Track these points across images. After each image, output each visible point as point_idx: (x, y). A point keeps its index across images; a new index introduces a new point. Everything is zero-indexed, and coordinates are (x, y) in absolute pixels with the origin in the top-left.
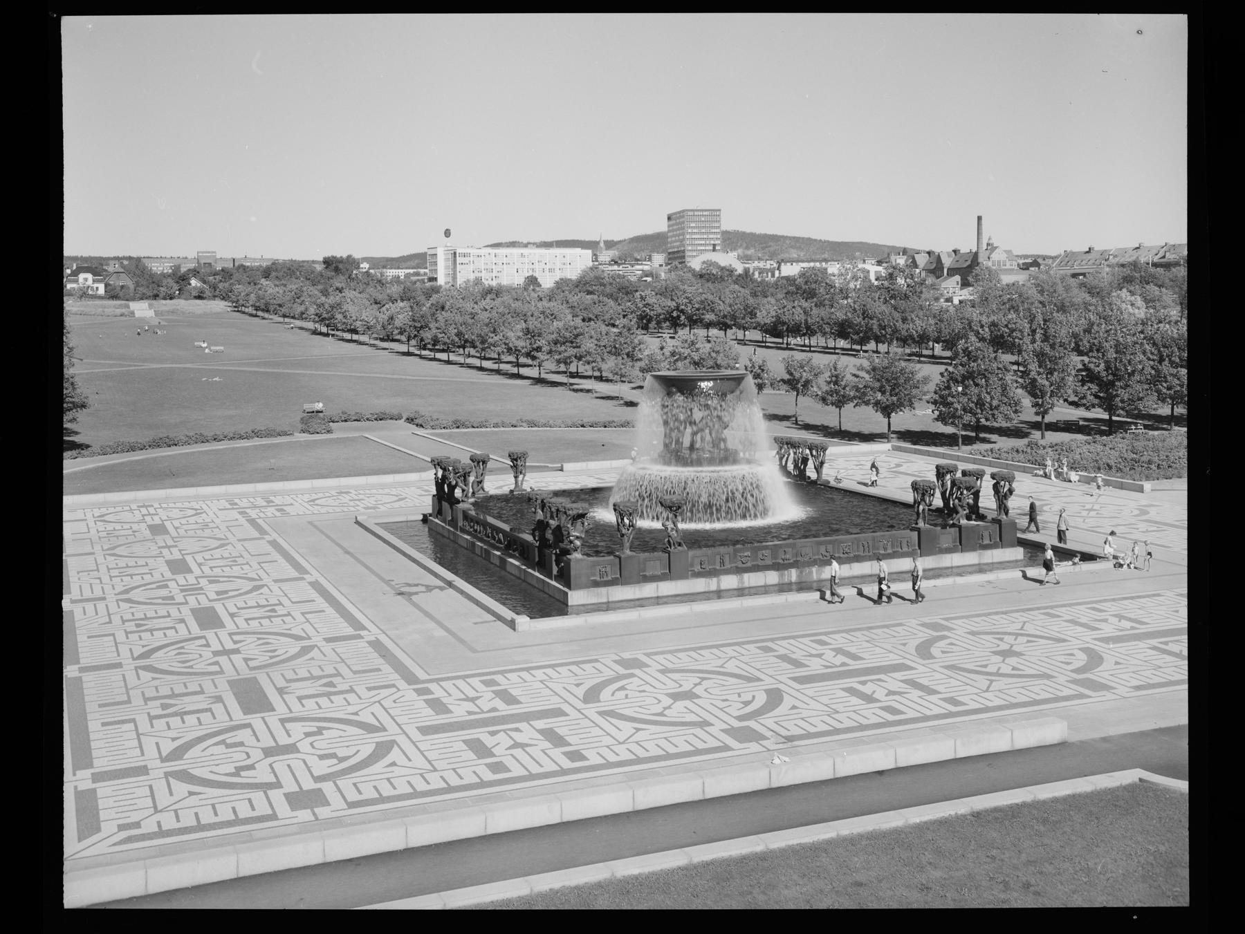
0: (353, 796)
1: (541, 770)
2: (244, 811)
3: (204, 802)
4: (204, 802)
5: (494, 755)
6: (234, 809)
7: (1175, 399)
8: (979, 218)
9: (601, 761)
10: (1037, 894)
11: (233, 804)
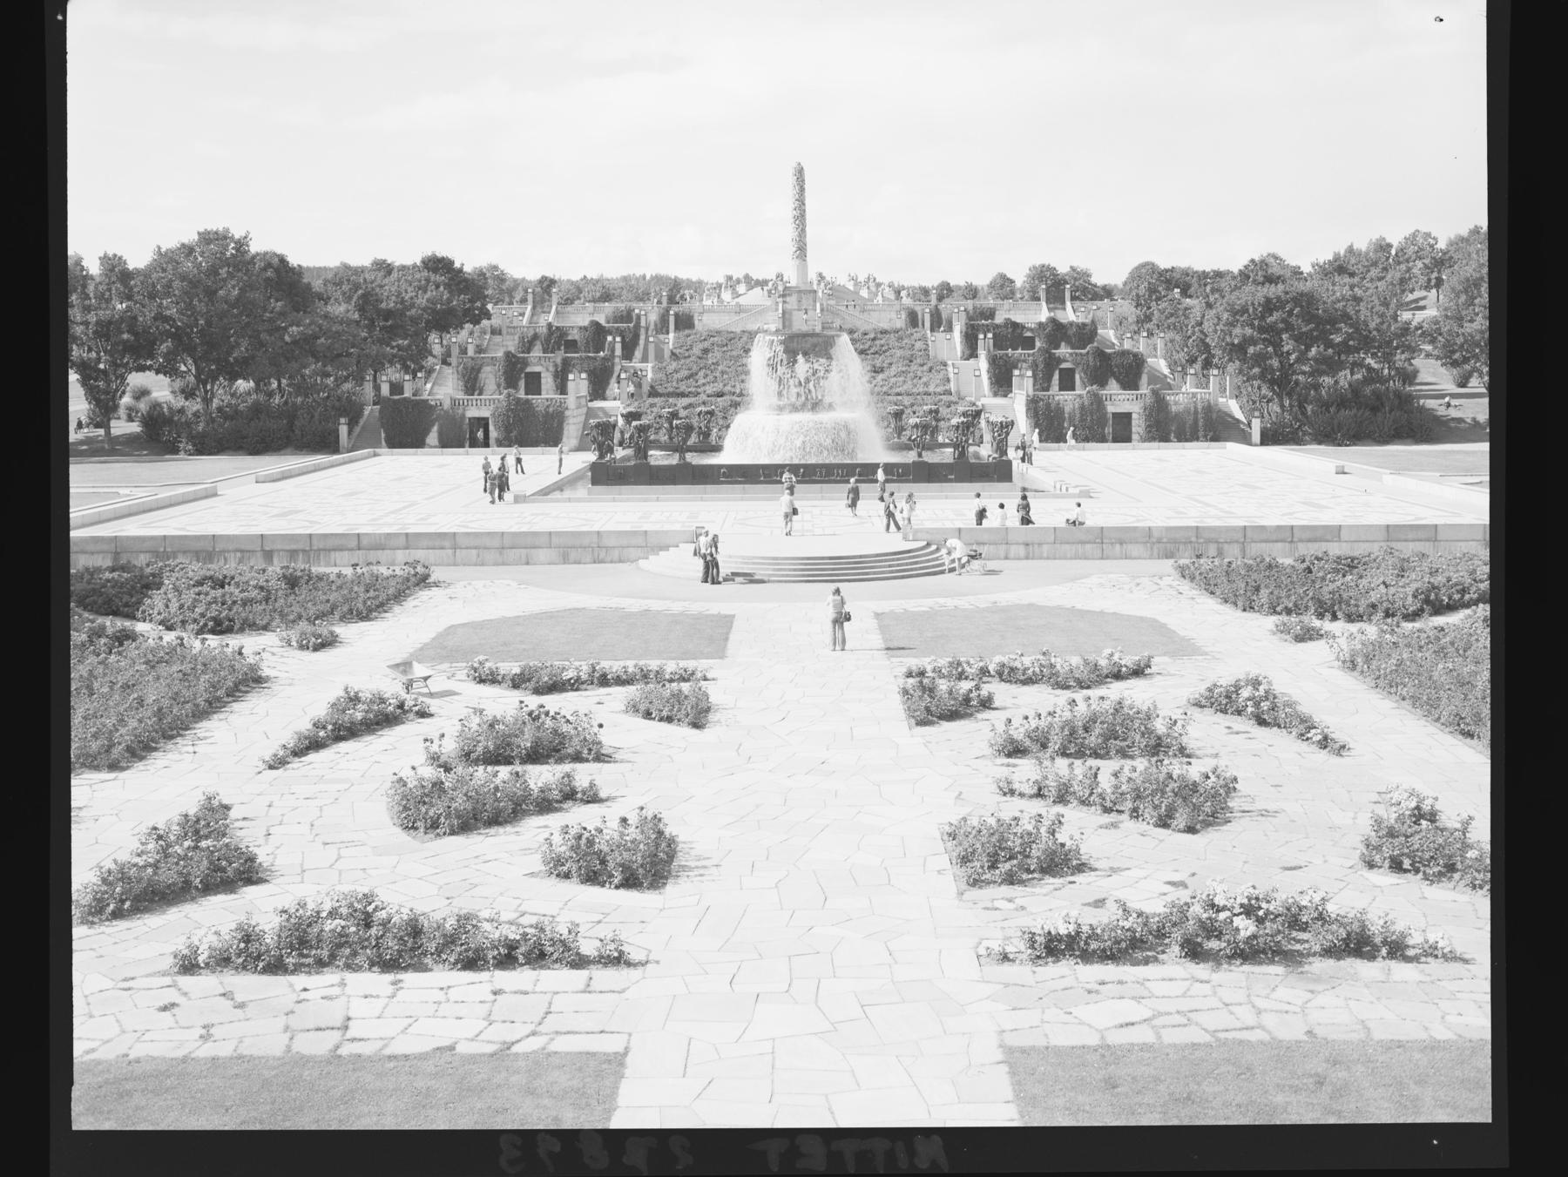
8: (800, 173)
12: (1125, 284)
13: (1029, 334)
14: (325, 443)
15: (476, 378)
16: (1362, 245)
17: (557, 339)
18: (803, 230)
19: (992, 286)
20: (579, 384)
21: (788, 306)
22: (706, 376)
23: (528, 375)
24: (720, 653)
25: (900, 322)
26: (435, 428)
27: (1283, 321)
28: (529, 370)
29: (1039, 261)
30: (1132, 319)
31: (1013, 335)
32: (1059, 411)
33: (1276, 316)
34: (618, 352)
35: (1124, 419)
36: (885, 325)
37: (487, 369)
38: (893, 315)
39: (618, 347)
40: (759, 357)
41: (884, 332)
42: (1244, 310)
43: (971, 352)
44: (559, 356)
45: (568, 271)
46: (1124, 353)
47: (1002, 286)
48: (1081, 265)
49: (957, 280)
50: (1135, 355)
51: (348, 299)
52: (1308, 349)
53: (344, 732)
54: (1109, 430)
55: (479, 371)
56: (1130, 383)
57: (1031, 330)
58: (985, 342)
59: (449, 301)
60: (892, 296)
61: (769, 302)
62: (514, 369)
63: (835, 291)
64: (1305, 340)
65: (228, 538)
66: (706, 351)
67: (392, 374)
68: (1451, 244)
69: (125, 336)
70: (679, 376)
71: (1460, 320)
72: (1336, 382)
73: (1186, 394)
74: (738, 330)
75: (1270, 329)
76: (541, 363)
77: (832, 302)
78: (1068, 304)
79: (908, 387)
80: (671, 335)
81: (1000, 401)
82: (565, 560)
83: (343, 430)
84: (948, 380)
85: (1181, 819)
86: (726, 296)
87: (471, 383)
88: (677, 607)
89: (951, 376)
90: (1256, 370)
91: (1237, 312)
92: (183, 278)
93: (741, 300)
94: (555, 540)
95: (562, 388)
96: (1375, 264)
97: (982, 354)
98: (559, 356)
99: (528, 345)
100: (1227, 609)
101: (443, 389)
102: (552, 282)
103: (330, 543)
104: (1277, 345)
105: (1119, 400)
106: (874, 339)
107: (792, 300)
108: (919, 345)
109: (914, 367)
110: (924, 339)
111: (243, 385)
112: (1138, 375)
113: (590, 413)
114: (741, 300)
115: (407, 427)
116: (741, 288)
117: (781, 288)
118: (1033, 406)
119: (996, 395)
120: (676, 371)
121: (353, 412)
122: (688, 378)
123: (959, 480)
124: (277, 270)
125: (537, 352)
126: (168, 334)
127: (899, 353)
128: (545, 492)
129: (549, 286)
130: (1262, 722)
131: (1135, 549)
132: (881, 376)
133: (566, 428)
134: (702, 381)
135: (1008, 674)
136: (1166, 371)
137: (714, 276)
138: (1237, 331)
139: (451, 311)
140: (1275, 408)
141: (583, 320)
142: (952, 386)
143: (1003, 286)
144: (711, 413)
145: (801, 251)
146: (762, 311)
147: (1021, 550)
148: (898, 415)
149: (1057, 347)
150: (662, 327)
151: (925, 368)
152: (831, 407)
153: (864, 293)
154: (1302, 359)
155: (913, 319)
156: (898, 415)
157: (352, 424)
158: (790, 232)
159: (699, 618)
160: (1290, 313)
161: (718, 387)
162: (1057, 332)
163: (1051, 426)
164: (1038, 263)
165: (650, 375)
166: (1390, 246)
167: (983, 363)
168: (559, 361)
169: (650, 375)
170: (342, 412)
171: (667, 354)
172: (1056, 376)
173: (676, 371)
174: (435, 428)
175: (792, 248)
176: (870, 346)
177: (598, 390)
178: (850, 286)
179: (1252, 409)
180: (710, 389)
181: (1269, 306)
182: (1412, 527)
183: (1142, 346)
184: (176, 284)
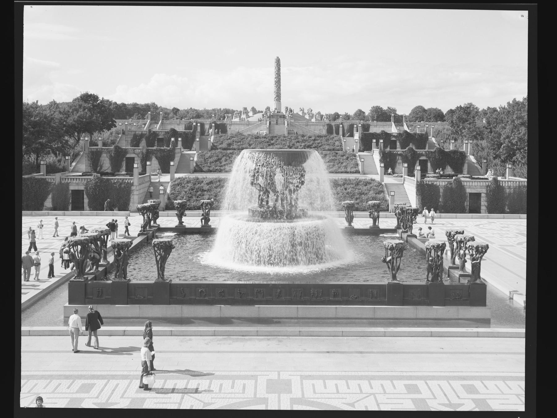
0: (250, 383)
1: (439, 382)
2: (319, 384)
3: (344, 396)
4: (344, 396)
5: (473, 400)
6: (325, 387)
7: (525, 178)
8: (278, 61)
9: (486, 382)
10: (235, 216)
11: (348, 391)
12: (410, 114)
13: (394, 139)
15: (98, 160)
19: (355, 114)
22: (226, 160)
23: (128, 158)
25: (324, 132)
26: (50, 196)
28: (128, 156)
36: (317, 132)
37: (104, 155)
41: (320, 136)
45: (166, 101)
47: (360, 115)
48: (392, 107)
49: (342, 112)
54: (467, 204)
57: (394, 136)
59: (91, 117)
60: (320, 119)
63: (295, 117)
70: (211, 160)
77: (292, 121)
84: (357, 165)
86: (243, 116)
89: (360, 163)
93: (250, 119)
102: (178, 110)
106: (314, 140)
109: (338, 157)
110: (340, 140)
112: (462, 164)
114: (250, 119)
116: (251, 114)
117: (268, 114)
120: (210, 157)
122: (216, 161)
129: (176, 112)
133: (132, 197)
134: (223, 163)
137: (239, 108)
151: (345, 157)
152: (304, 215)
153: (307, 117)
158: (272, 88)
164: (375, 105)
165: (196, 159)
169: (196, 159)
173: (210, 157)
174: (50, 196)
175: (274, 96)
178: (301, 113)
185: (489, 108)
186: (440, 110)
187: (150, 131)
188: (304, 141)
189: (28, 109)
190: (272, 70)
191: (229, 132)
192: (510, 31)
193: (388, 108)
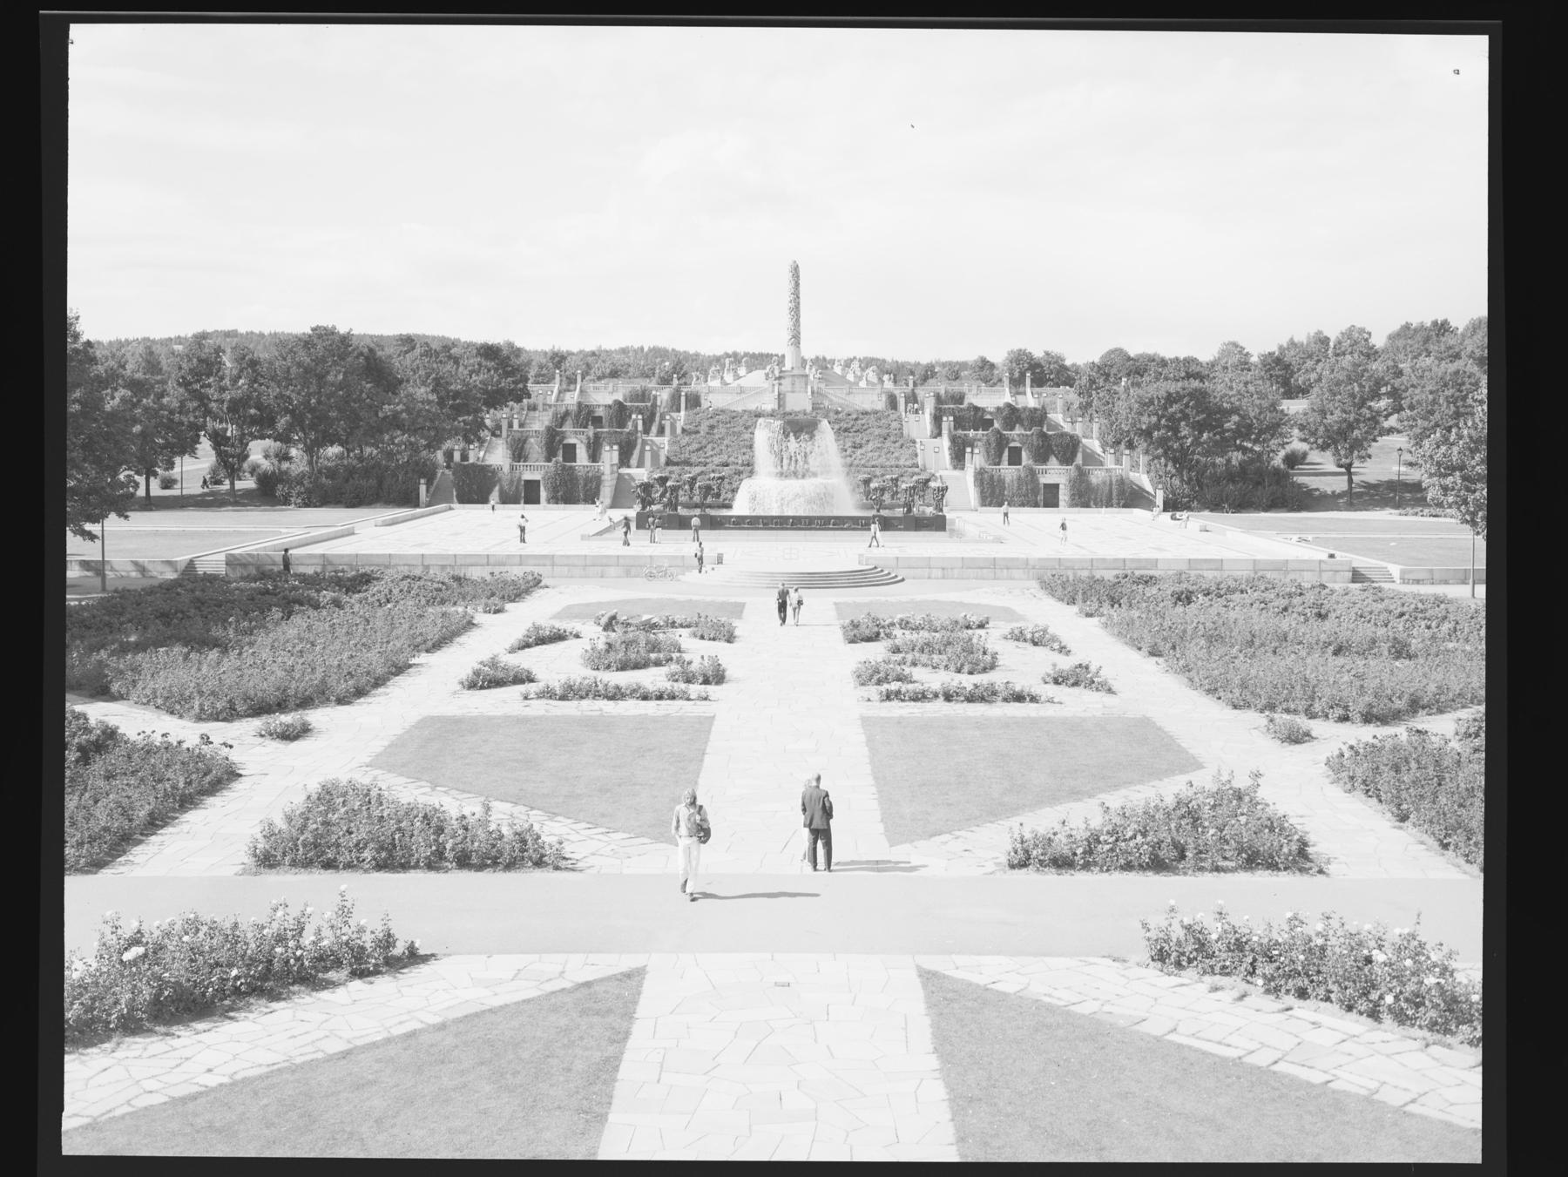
8: (796, 271)
14: (408, 499)
15: (522, 448)
16: (1301, 338)
17: (586, 416)
18: (798, 320)
20: (610, 455)
21: (783, 388)
24: (740, 617)
25: (880, 404)
27: (1181, 411)
29: (1017, 345)
30: (1076, 405)
31: (978, 418)
32: (1001, 481)
33: (1175, 408)
34: (640, 428)
35: (1053, 489)
36: (868, 407)
38: (875, 398)
39: (640, 423)
40: (764, 436)
42: (1151, 402)
43: (938, 434)
44: (590, 431)
46: (1063, 435)
47: (982, 368)
50: (1072, 437)
51: (424, 383)
52: (1201, 433)
53: (541, 641)
54: (1040, 498)
55: (525, 442)
56: (1067, 459)
58: (947, 422)
59: (499, 382)
61: (766, 385)
62: (554, 443)
64: (1200, 427)
65: (400, 556)
66: (712, 427)
67: (455, 445)
68: (1392, 337)
69: (253, 411)
71: (1323, 413)
72: (1229, 461)
73: (1112, 466)
74: (740, 409)
75: (1171, 418)
76: (578, 439)
78: (1028, 390)
79: (882, 460)
80: (683, 413)
81: (957, 473)
82: (628, 574)
83: (423, 488)
85: (966, 669)
87: (519, 452)
88: (709, 599)
90: (1160, 451)
91: (1146, 404)
92: (299, 365)
94: (621, 561)
95: (594, 456)
96: (1310, 357)
97: (945, 432)
98: (590, 431)
99: (562, 419)
100: (1060, 604)
101: (497, 456)
103: (468, 561)
104: (1176, 431)
105: (1055, 473)
107: (786, 382)
108: (895, 425)
109: (888, 444)
110: (899, 419)
111: (334, 450)
112: (1074, 455)
113: (620, 477)
115: (475, 487)
118: (980, 476)
119: (955, 468)
121: (429, 473)
123: (906, 529)
124: (367, 358)
125: (568, 428)
126: (287, 411)
127: (877, 431)
128: (600, 533)
130: (1035, 644)
131: (1016, 573)
132: (859, 451)
135: (905, 624)
136: (1099, 450)
138: (1145, 419)
139: (500, 392)
140: (1176, 481)
141: (608, 399)
142: (920, 460)
143: (985, 371)
144: (722, 478)
145: (796, 338)
146: (759, 392)
147: (939, 573)
148: (867, 482)
149: (1012, 429)
150: (675, 405)
154: (1196, 442)
155: (892, 402)
156: (867, 482)
157: (429, 484)
158: (786, 321)
159: (723, 604)
160: (1187, 406)
161: (724, 458)
162: (1012, 416)
163: (992, 493)
166: (1327, 339)
167: (945, 442)
168: (591, 434)
170: (422, 475)
171: (679, 431)
172: (1006, 453)
176: (851, 427)
177: (624, 460)
179: (1158, 480)
180: (717, 460)
181: (1171, 399)
182: (1206, 561)
183: (1078, 430)
184: (294, 370)
185: (1292, 343)
186: (323, 334)
187: (579, 404)
188: (839, 421)
189: (494, 846)
190: (787, 286)
191: (705, 404)
192: (1418, 114)
193: (1047, 354)
